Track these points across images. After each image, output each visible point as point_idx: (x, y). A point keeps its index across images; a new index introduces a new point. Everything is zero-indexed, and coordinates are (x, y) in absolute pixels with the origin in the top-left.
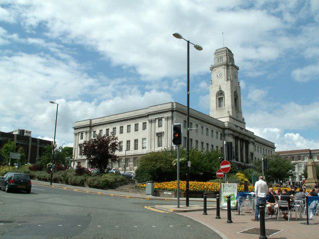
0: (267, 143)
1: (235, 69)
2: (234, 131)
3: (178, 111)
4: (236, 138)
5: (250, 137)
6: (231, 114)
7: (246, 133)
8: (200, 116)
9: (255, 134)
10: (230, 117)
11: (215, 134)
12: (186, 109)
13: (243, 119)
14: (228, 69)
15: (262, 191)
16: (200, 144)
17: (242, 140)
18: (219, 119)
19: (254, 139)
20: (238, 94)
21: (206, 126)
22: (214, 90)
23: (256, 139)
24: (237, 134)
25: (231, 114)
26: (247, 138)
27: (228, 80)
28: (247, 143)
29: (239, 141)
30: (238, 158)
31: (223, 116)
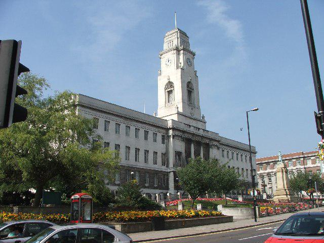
0: (240, 146)
1: (190, 56)
2: (184, 132)
3: (83, 106)
4: (188, 142)
5: (211, 139)
6: (181, 110)
7: (205, 134)
8: (123, 113)
9: (220, 135)
10: (179, 113)
11: (150, 135)
12: (248, 148)
13: (203, 117)
14: (178, 54)
15: (12, 211)
16: (123, 151)
17: (198, 144)
18: (163, 118)
19: (218, 141)
20: (194, 85)
21: (226, 149)
22: (162, 83)
23: (223, 141)
24: (186, 136)
25: (181, 110)
26: (207, 141)
27: (177, 67)
28: (207, 147)
29: (192, 145)
30: (168, 160)
31: (168, 111)
